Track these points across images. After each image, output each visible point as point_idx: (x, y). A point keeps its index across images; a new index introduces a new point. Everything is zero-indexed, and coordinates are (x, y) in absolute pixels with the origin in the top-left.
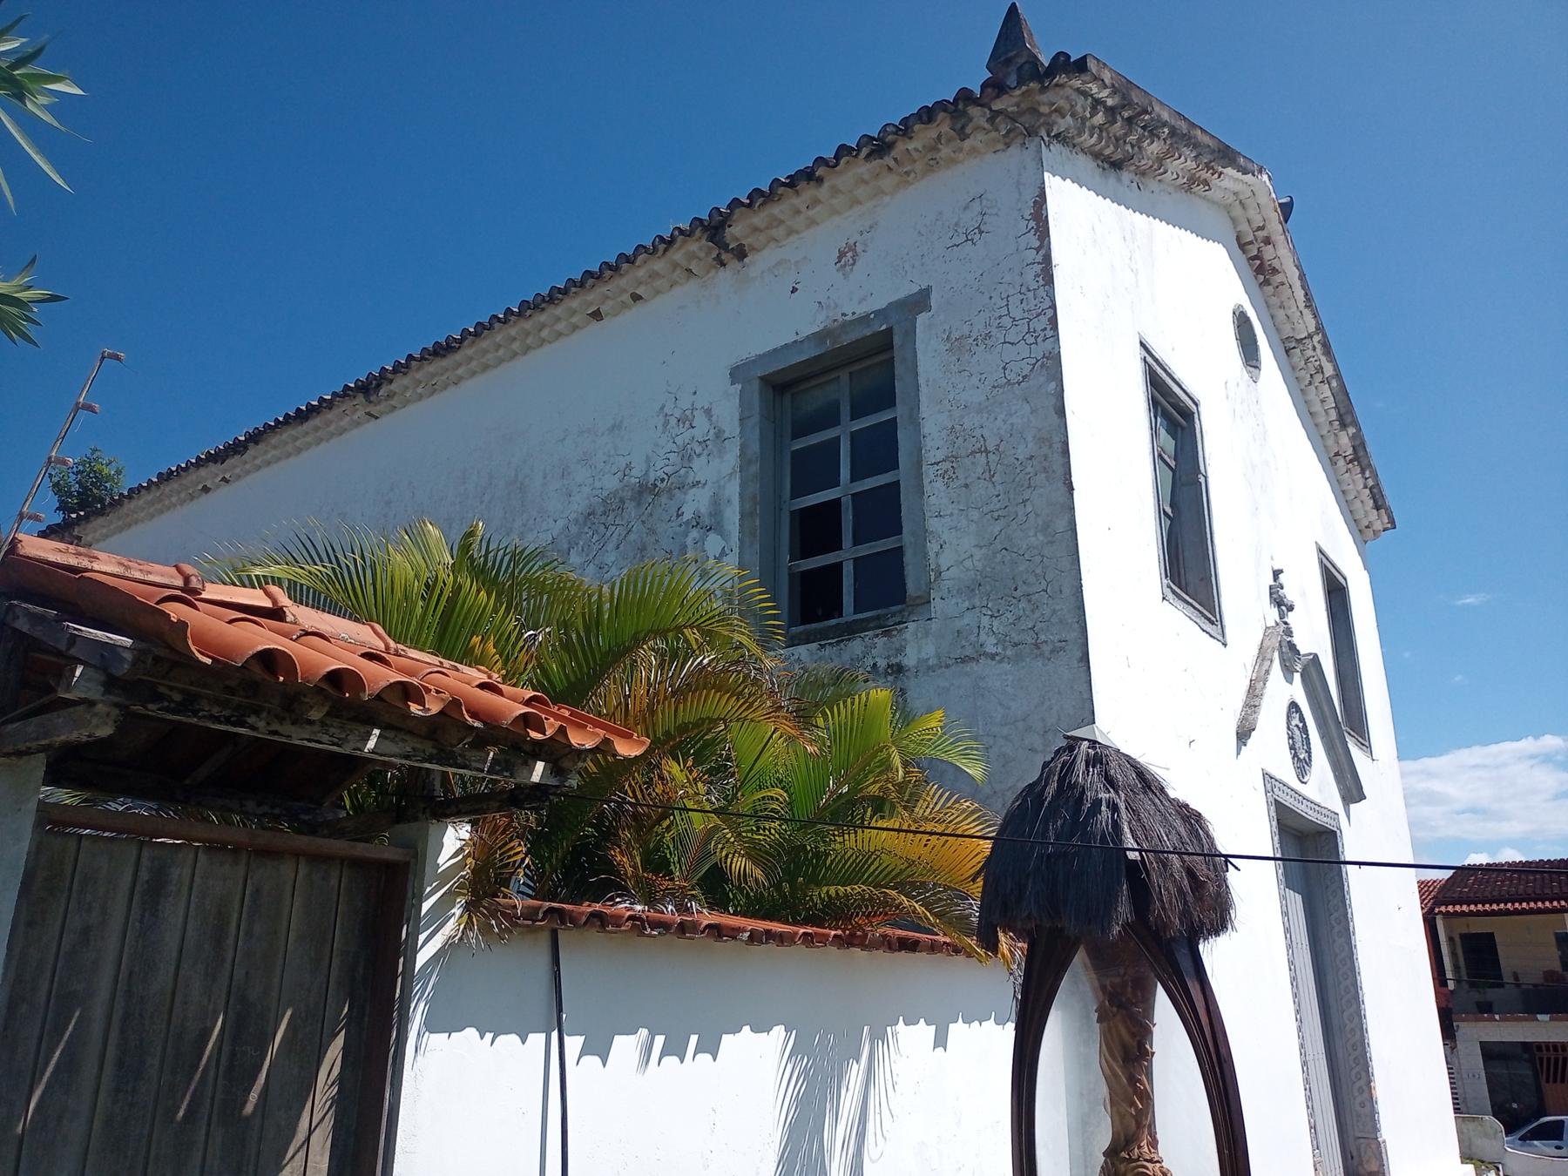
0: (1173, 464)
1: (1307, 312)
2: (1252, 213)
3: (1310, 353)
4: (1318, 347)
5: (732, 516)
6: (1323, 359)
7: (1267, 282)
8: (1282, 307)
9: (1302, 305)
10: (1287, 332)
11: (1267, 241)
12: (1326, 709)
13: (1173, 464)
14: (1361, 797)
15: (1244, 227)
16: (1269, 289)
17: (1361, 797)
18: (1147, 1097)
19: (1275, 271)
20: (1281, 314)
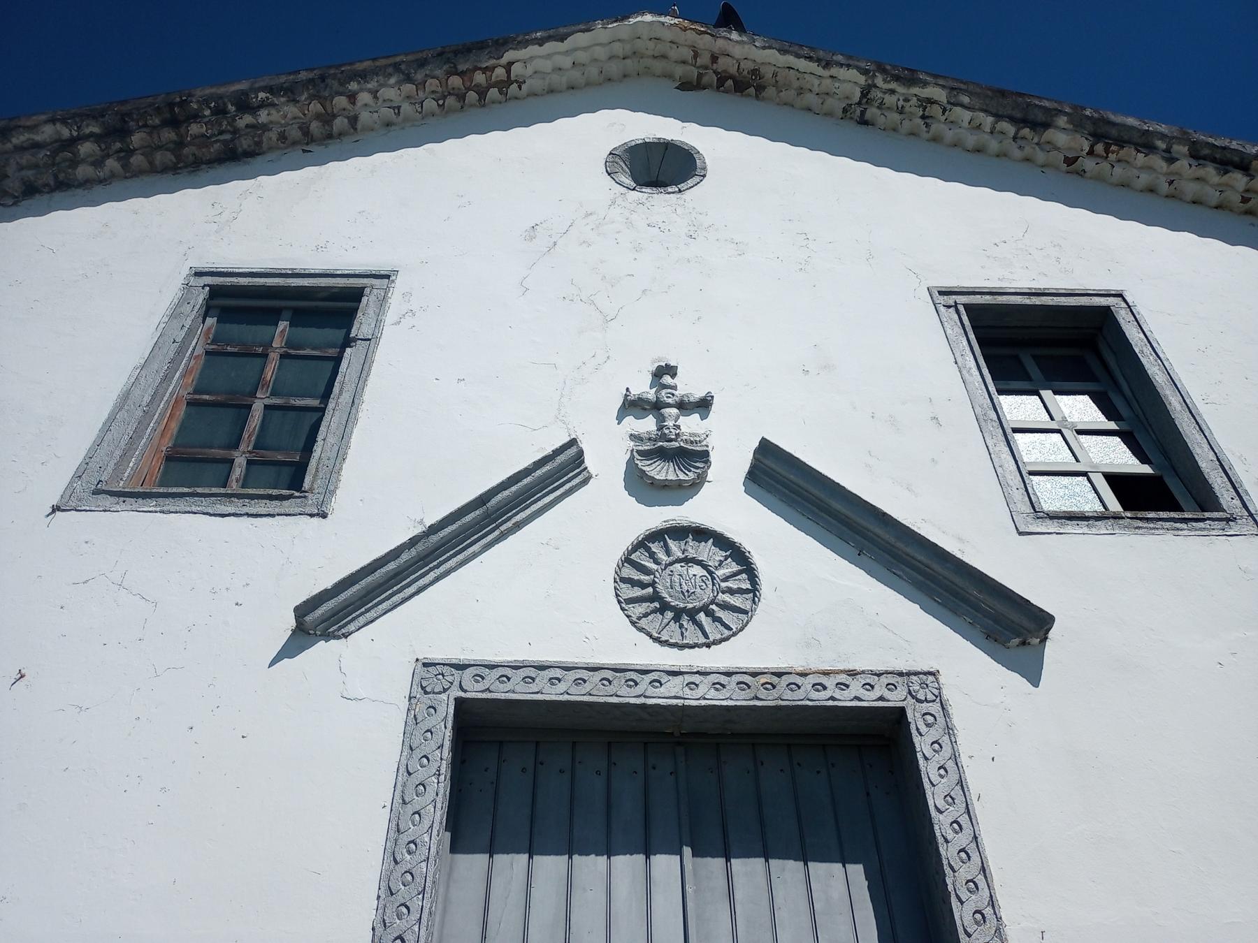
0: (1112, 426)
1: (835, 71)
2: (674, 53)
3: (890, 100)
4: (893, 85)
5: (447, 744)
6: (915, 90)
7: (760, 89)
8: (800, 91)
9: (820, 71)
10: (837, 105)
11: (714, 59)
12: (837, 505)
13: (1112, 426)
14: (1041, 622)
15: (679, 71)
16: (771, 91)
17: (1041, 622)
18: (358, 571)
19: (755, 72)
20: (810, 99)
